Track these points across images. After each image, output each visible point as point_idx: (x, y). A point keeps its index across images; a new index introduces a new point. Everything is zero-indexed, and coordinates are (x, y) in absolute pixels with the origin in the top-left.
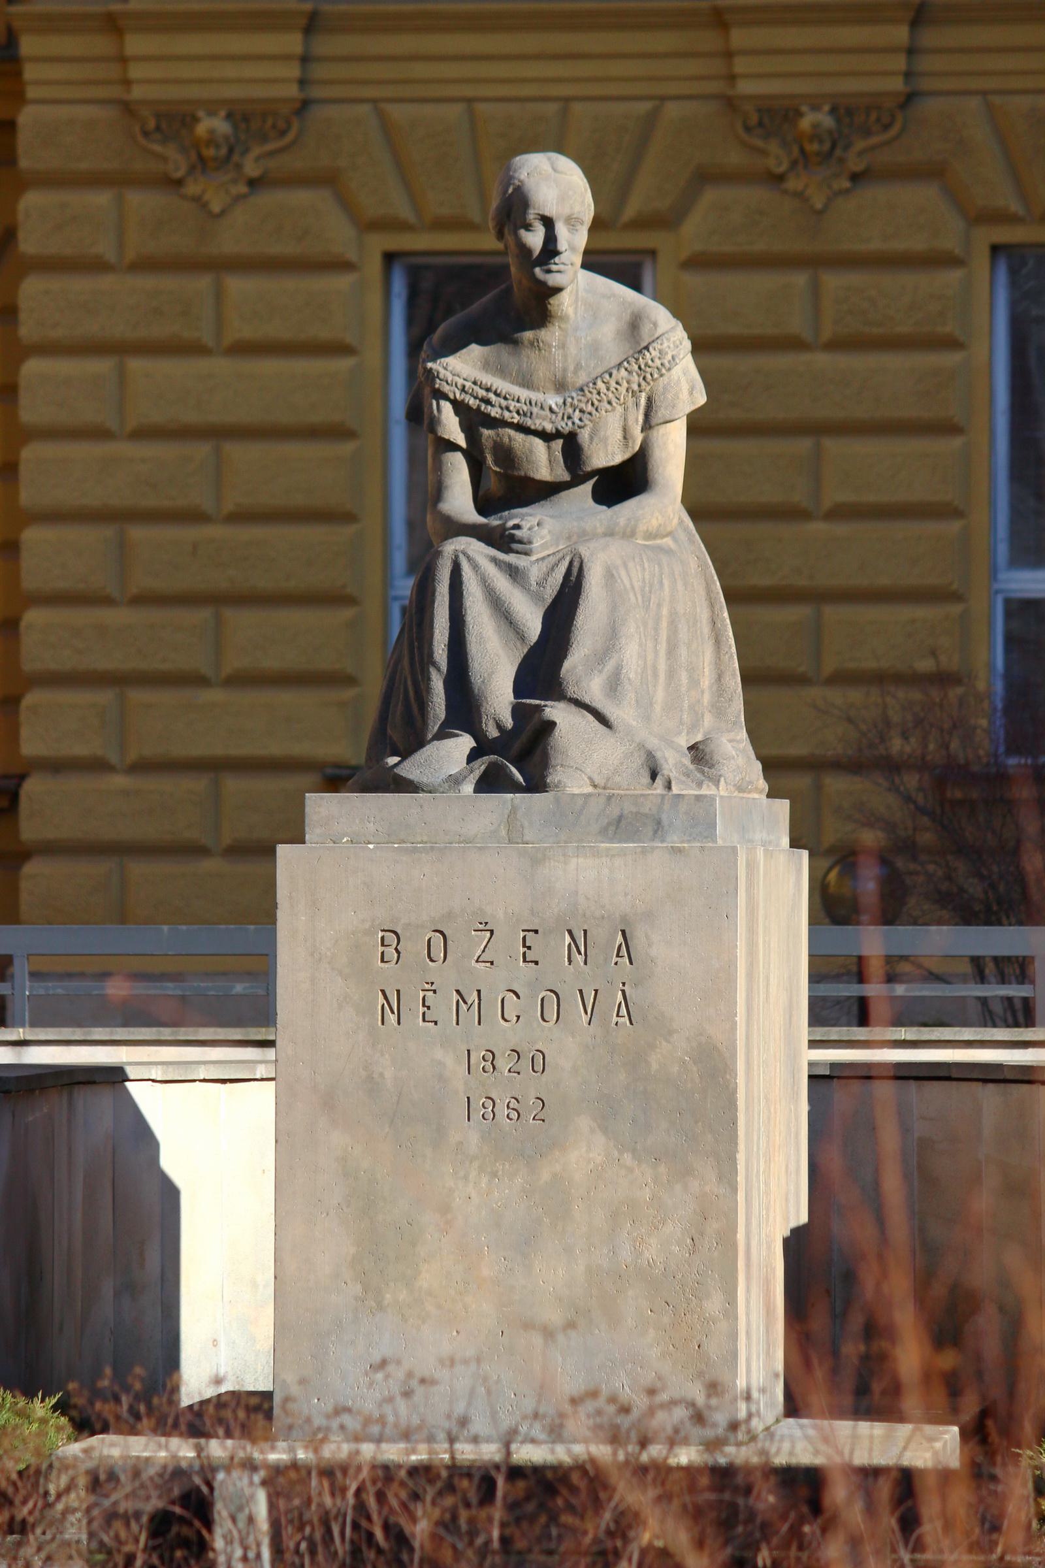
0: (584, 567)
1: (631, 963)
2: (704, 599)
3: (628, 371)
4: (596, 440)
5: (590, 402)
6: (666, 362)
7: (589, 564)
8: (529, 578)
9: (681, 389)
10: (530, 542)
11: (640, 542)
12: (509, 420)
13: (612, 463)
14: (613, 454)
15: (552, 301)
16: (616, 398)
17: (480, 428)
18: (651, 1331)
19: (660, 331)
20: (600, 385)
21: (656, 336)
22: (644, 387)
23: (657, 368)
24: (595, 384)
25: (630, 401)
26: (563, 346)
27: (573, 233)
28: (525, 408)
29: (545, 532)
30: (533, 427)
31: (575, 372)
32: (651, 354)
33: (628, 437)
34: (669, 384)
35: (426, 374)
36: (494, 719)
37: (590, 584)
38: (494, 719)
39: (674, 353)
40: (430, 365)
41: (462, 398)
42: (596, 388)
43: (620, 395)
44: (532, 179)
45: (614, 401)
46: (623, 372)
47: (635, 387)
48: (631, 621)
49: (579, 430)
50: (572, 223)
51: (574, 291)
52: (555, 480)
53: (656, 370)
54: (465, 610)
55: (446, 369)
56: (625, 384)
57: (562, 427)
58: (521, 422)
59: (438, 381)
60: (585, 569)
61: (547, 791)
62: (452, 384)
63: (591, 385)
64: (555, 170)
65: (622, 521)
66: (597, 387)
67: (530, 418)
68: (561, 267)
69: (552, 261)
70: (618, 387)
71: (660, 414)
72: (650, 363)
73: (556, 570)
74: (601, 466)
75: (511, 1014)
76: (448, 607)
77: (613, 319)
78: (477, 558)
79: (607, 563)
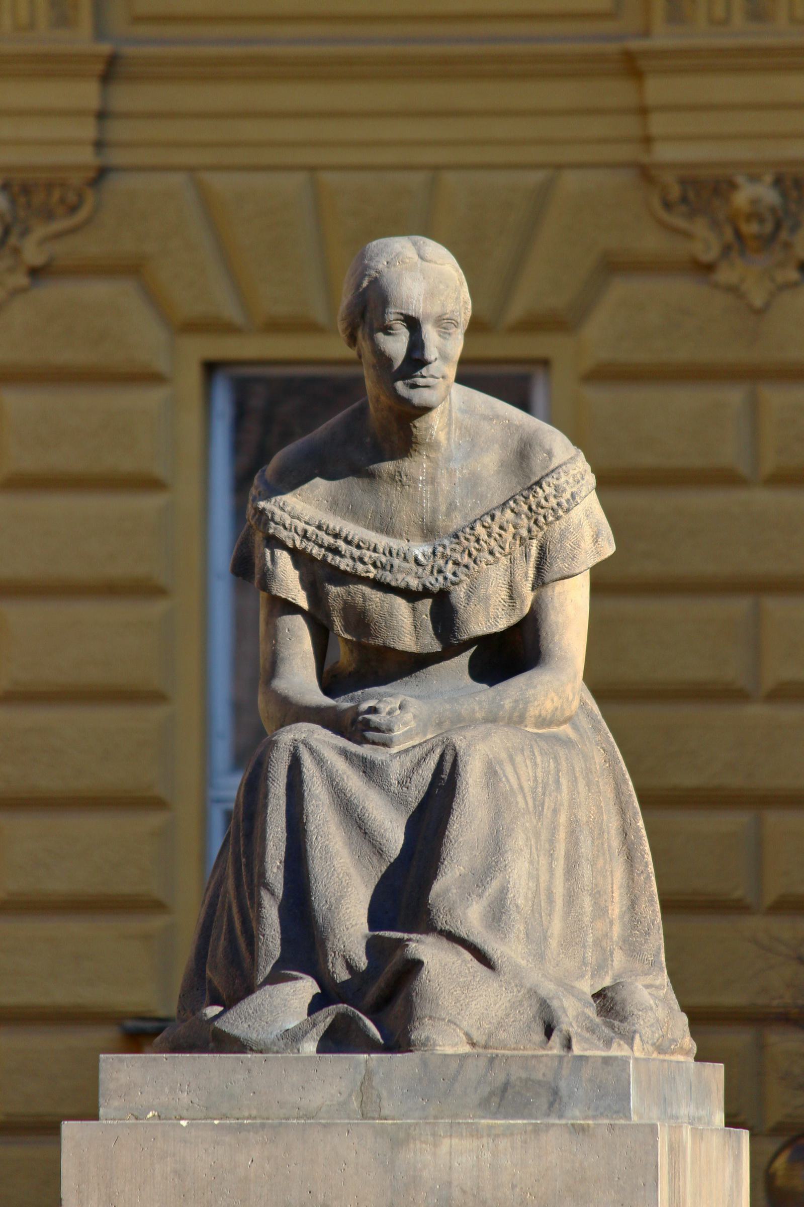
3: (515, 513)
4: (474, 599)
5: (467, 552)
6: (563, 501)
7: (466, 758)
9: (583, 537)
10: (390, 730)
11: (531, 730)
12: (364, 575)
14: (496, 618)
15: (417, 423)
19: (555, 463)
21: (552, 467)
23: (552, 509)
24: (472, 528)
25: (518, 551)
26: (432, 480)
27: (445, 338)
28: (384, 559)
30: (393, 584)
31: (448, 514)
32: (544, 491)
33: (515, 596)
34: (567, 529)
37: (467, 784)
39: (574, 490)
40: (262, 504)
41: (303, 547)
42: (474, 535)
44: (392, 269)
45: (497, 549)
46: (509, 515)
47: (524, 533)
50: (444, 325)
51: (447, 412)
52: (421, 651)
53: (551, 511)
55: (282, 509)
56: (511, 529)
57: (432, 585)
58: (379, 576)
59: (272, 524)
60: (461, 765)
61: (411, 1051)
63: (468, 530)
64: (422, 258)
65: (508, 704)
67: (390, 571)
68: (430, 381)
69: (419, 373)
70: (502, 532)
72: (543, 502)
73: (423, 766)
74: (480, 633)
77: (496, 446)
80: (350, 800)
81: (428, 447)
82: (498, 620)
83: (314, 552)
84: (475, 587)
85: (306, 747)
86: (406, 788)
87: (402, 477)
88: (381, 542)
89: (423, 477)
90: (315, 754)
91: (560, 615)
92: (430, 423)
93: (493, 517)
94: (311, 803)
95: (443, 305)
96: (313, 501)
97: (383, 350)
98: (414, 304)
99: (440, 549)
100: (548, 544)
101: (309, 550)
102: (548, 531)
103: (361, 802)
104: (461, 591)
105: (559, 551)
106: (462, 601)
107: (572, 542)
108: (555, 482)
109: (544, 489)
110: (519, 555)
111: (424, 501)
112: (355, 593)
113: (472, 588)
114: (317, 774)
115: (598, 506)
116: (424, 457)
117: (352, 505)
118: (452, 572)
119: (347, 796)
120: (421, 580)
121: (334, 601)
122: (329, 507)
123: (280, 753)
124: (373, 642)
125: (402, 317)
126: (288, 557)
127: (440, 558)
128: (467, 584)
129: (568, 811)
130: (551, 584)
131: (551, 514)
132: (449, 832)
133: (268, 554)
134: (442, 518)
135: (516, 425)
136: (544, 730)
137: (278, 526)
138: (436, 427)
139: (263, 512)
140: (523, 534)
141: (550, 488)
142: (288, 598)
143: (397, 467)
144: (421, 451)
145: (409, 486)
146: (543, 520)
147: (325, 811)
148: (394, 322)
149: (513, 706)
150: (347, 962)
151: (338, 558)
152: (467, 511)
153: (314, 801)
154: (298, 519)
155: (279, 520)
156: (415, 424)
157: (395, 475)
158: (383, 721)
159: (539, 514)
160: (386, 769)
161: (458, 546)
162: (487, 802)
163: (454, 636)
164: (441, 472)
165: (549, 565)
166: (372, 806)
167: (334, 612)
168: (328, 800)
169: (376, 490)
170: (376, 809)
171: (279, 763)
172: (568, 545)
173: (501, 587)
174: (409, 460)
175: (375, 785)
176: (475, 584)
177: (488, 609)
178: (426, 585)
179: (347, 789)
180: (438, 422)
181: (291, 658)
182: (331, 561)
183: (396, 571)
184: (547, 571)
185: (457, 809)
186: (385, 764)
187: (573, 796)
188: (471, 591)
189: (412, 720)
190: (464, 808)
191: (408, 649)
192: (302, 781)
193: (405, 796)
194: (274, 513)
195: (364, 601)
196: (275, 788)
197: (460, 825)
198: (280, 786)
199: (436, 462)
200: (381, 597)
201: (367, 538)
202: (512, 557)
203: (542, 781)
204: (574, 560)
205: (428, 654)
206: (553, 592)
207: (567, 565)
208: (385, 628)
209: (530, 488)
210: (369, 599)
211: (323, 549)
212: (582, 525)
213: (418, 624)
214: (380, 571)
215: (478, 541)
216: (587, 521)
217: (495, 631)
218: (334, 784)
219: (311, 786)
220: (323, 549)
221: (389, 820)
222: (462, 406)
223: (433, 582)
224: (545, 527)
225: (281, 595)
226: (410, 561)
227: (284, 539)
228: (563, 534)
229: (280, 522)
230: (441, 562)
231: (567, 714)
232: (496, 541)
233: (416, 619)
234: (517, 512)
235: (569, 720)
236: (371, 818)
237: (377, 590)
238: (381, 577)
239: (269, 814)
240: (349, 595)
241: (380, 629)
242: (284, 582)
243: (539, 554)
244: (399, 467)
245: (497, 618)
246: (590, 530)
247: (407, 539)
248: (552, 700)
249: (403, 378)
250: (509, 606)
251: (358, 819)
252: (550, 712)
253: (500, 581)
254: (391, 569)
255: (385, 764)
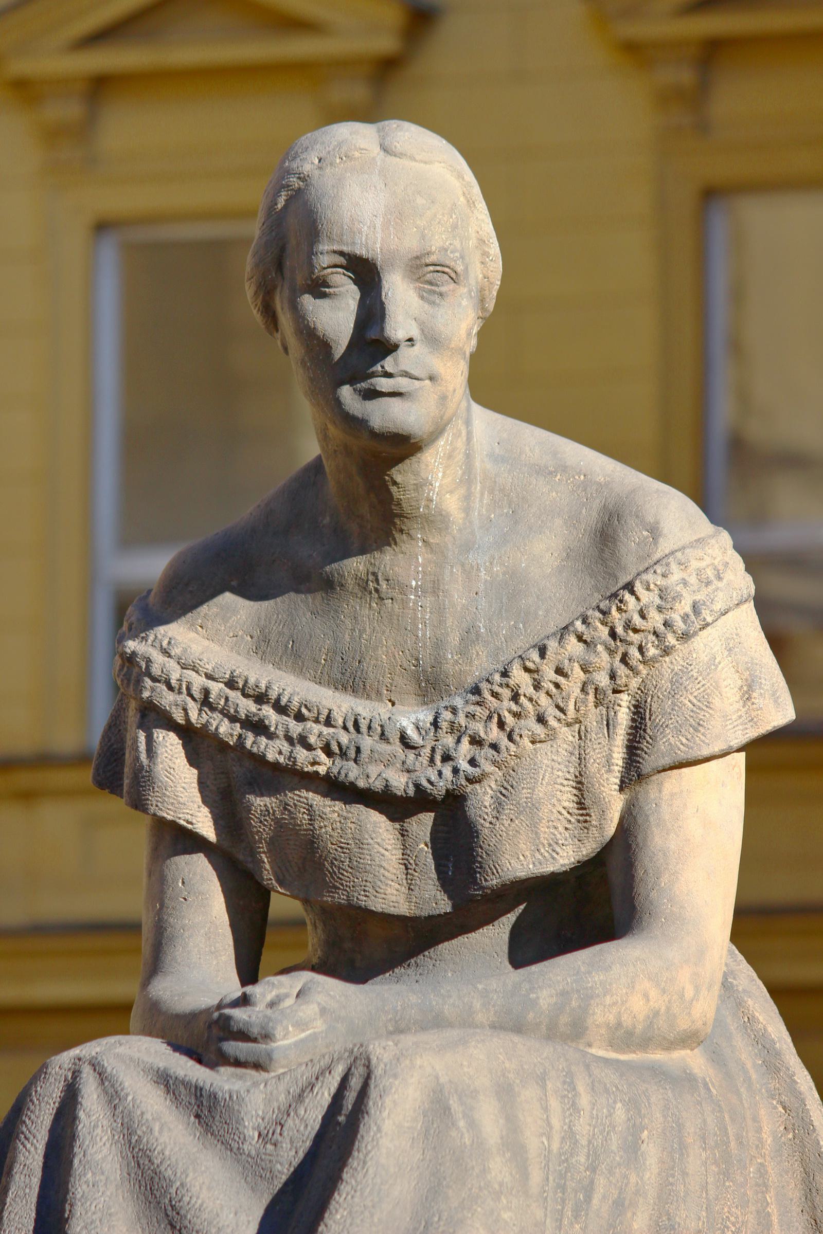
0: (372, 1086)
2: (796, 1209)
3: (585, 642)
4: (509, 809)
5: (495, 719)
6: (676, 618)
7: (385, 1082)
8: (240, 1121)
9: (717, 687)
10: (267, 1037)
11: (601, 1053)
12: (310, 769)
13: (550, 868)
14: (554, 845)
15: (399, 474)
16: (558, 707)
17: (251, 797)
19: (665, 546)
20: (519, 677)
21: (658, 555)
22: (624, 680)
23: (655, 633)
24: (505, 674)
25: (593, 715)
26: (434, 587)
27: (432, 303)
28: (344, 739)
29: (309, 1010)
30: (361, 784)
31: (463, 651)
32: (638, 599)
33: (588, 802)
34: (685, 671)
37: (379, 1130)
39: (698, 597)
40: (132, 645)
41: (203, 721)
42: (508, 686)
43: (566, 699)
44: (328, 170)
45: (551, 713)
46: (573, 646)
47: (603, 680)
48: (477, 1225)
49: (469, 788)
50: (429, 277)
51: (460, 457)
52: (418, 913)
53: (652, 638)
54: (71, 1205)
55: (166, 653)
56: (578, 674)
57: (429, 781)
58: (335, 771)
59: (148, 682)
60: (373, 1093)
62: (180, 688)
63: (497, 678)
64: (385, 149)
65: (545, 998)
66: (511, 682)
67: (356, 761)
68: (401, 383)
69: (378, 368)
70: (561, 680)
71: (662, 746)
72: (637, 620)
73: (307, 1101)
74: (522, 874)
76: (34, 1199)
77: (558, 522)
78: (122, 1075)
79: (437, 1078)
80: (158, 1171)
81: (425, 524)
82: (558, 849)
83: (222, 730)
84: (512, 786)
85: (95, 1070)
86: (271, 1144)
87: (380, 582)
88: (339, 707)
89: (417, 582)
90: (106, 1084)
91: (672, 835)
92: (423, 474)
93: (543, 652)
94: (83, 1179)
95: (423, 237)
96: (227, 638)
97: (312, 326)
98: (364, 234)
100: (649, 700)
101: (213, 728)
102: (649, 677)
103: (178, 1175)
104: (485, 793)
105: (670, 713)
106: (487, 813)
107: (695, 697)
108: (660, 581)
109: (638, 594)
110: (595, 723)
111: (420, 626)
112: (294, 804)
113: (505, 789)
114: (105, 1123)
115: (757, 633)
116: (420, 544)
117: (293, 642)
118: (468, 758)
119: (153, 1164)
120: (413, 775)
121: (261, 822)
122: (254, 648)
123: (48, 1084)
124: (329, 899)
125: (341, 260)
126: (178, 743)
127: (447, 733)
128: (496, 781)
129: (656, 1208)
130: (654, 778)
131: (653, 642)
132: (326, 1226)
133: (143, 738)
134: (452, 657)
135: (599, 484)
136: (634, 1055)
137: (158, 684)
138: (437, 484)
139: (130, 660)
140: (601, 682)
141: (651, 594)
142: (178, 821)
143: (371, 564)
144: (412, 532)
145: (392, 599)
146: (637, 655)
147: (108, 1193)
148: (330, 270)
149: (556, 1004)
151: (263, 740)
152: (498, 644)
153: (89, 1175)
154: (193, 670)
155: (160, 673)
156: (394, 477)
157: (368, 580)
158: (254, 1018)
159: (631, 644)
160: (236, 1107)
161: (478, 709)
162: (418, 1167)
163: (475, 882)
164: (452, 571)
165: (651, 741)
166: (201, 1181)
167: (262, 843)
168: (119, 1172)
169: (336, 611)
170: (209, 1189)
171: (43, 1104)
172: (687, 702)
173: (562, 784)
174: (392, 551)
175: (216, 1142)
176: (511, 779)
177: (535, 827)
178: (421, 785)
179: (155, 1149)
180: (440, 475)
181: (186, 934)
182: (252, 747)
183: (367, 760)
184: (646, 753)
185: (349, 1180)
186: (235, 1098)
187: (670, 1179)
188: (504, 793)
189: (318, 1017)
190: (364, 1177)
191: (392, 909)
192: (74, 1136)
193: (270, 1161)
194: (150, 661)
195: (310, 820)
196: (27, 1153)
197: (350, 1213)
198: (36, 1148)
199: (443, 552)
200: (342, 810)
201: (314, 700)
202: (583, 728)
203: (590, 1142)
204: (699, 731)
205: (430, 917)
206: (660, 792)
207: (684, 741)
208: (350, 870)
209: (615, 595)
210: (319, 816)
211: (238, 725)
212: (717, 666)
213: (412, 861)
214: (338, 761)
215: (515, 698)
216: (730, 658)
217: (552, 869)
218: (133, 1141)
219: (88, 1146)
220: (238, 725)
221: (233, 1209)
222: (497, 451)
223: (433, 779)
224: (641, 667)
225: (165, 815)
226: (391, 740)
227: (168, 708)
228: (677, 681)
229: (160, 676)
231: (683, 1024)
232: (551, 696)
233: (408, 852)
234: (589, 640)
235: (689, 1039)
236: (194, 1205)
237: (333, 799)
238: (339, 773)
239: (8, 1204)
240: (285, 809)
241: (341, 871)
242: (170, 789)
243: (633, 720)
244: (375, 565)
245: (555, 846)
246: (736, 676)
247: (390, 701)
248: (646, 996)
249: (352, 381)
250: (579, 821)
251: (170, 1208)
252: (641, 1020)
253: (560, 773)
254: (356, 757)
255: (235, 1098)
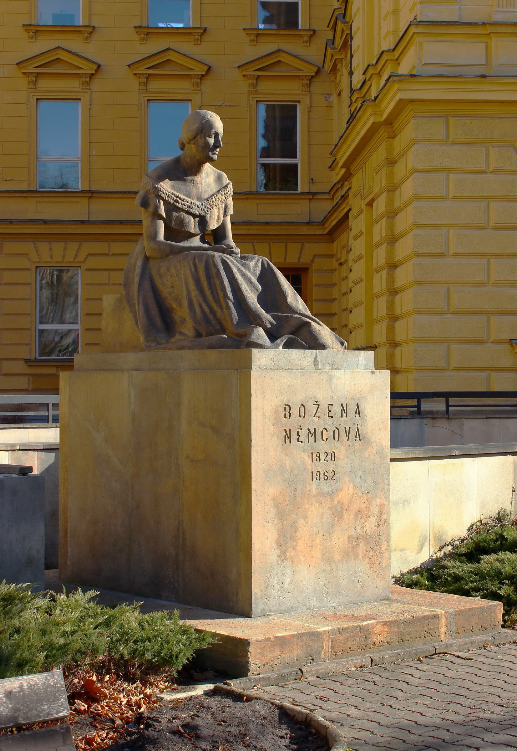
1: (360, 416)
18: (367, 559)
35: (154, 189)
36: (268, 321)
38: (268, 321)
61: (325, 349)
75: (325, 438)
93: (217, 195)
99: (204, 203)
150: (270, 322)
230: (204, 207)
